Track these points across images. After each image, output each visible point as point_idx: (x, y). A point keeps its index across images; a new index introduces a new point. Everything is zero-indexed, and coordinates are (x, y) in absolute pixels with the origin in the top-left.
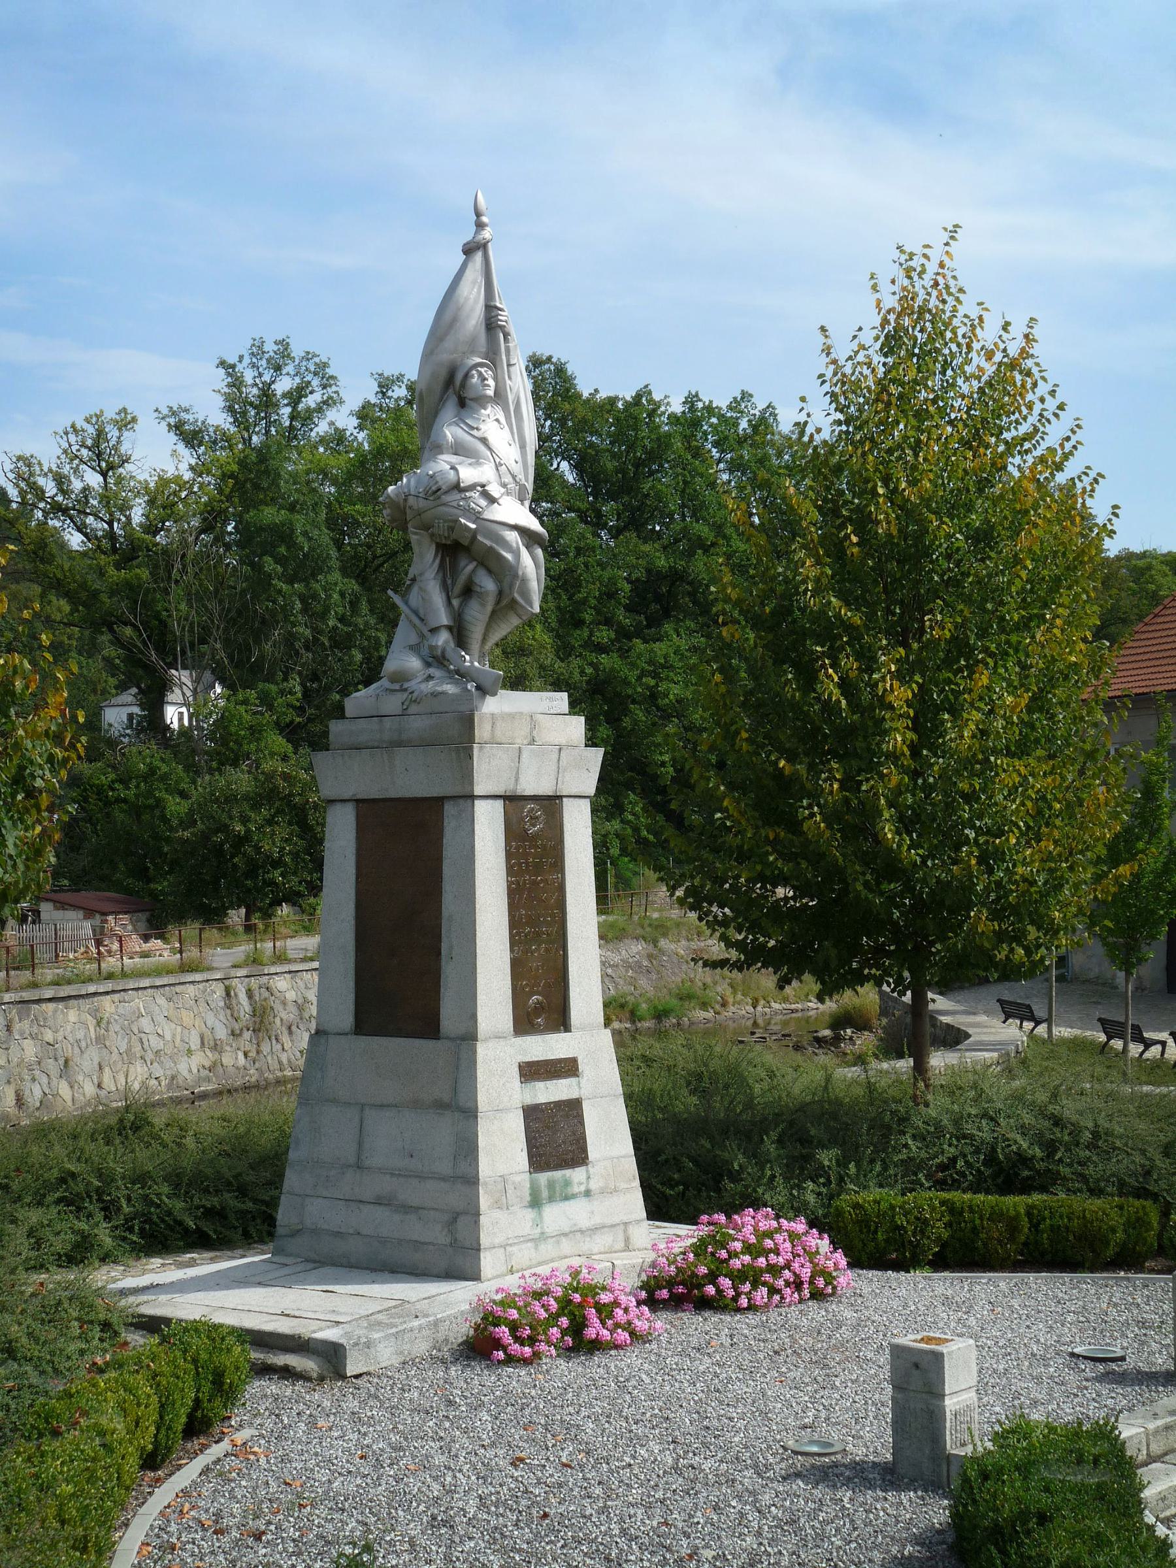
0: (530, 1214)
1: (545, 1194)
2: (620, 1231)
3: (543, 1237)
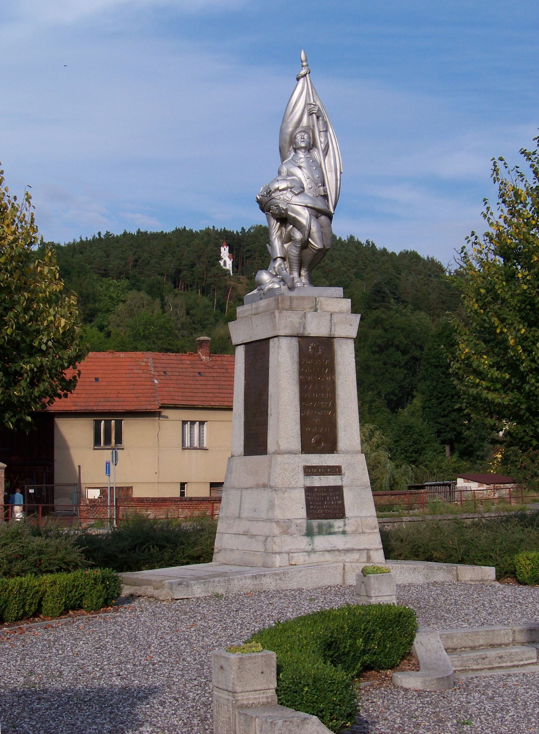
0: (306, 540)
1: (316, 530)
2: (364, 554)
3: (313, 551)
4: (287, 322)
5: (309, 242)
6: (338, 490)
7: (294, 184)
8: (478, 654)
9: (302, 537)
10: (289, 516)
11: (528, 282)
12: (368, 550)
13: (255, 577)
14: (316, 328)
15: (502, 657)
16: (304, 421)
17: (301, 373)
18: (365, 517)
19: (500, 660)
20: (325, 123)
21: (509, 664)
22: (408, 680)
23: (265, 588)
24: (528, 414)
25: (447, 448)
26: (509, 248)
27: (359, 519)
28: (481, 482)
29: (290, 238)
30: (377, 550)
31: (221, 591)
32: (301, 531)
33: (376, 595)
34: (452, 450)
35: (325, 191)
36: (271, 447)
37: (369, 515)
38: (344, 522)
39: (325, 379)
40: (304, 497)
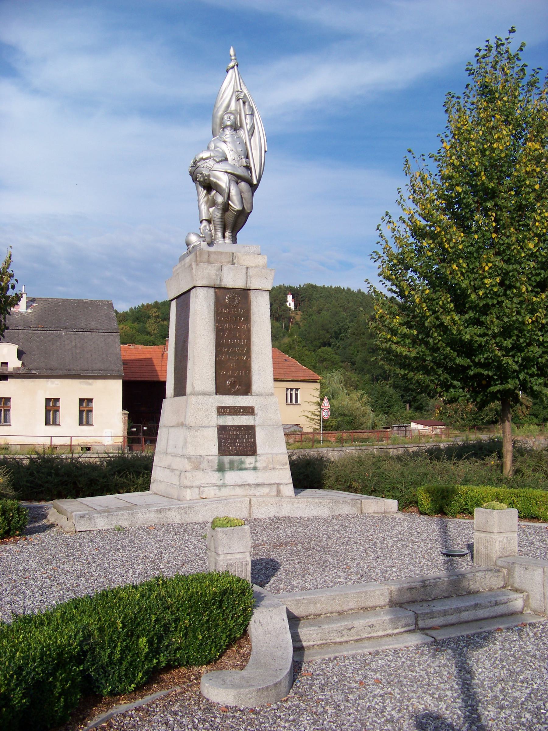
0: (217, 475)
1: (227, 466)
2: (275, 488)
3: (224, 486)
4: (204, 274)
5: (229, 204)
6: (251, 429)
7: (217, 154)
8: (343, 624)
9: (213, 473)
10: (201, 453)
11: (431, 250)
12: (278, 484)
13: (159, 511)
14: (232, 280)
15: (373, 625)
16: (219, 365)
17: (217, 321)
18: (276, 454)
19: (370, 630)
20: (251, 108)
21: (381, 633)
22: (219, 689)
23: (170, 521)
24: (432, 364)
25: (408, 405)
26: (419, 229)
27: (270, 456)
28: (425, 425)
29: (213, 203)
30: (287, 484)
31: (125, 524)
32: (212, 467)
33: (225, 552)
34: (410, 406)
35: (248, 163)
36: (189, 389)
37: (280, 452)
38: (256, 458)
39: (241, 327)
40: (216, 436)
